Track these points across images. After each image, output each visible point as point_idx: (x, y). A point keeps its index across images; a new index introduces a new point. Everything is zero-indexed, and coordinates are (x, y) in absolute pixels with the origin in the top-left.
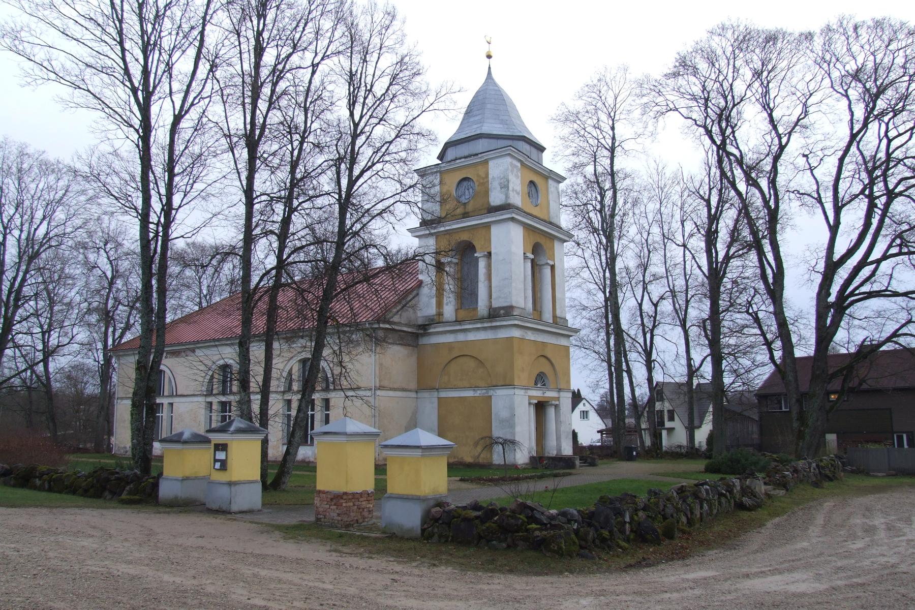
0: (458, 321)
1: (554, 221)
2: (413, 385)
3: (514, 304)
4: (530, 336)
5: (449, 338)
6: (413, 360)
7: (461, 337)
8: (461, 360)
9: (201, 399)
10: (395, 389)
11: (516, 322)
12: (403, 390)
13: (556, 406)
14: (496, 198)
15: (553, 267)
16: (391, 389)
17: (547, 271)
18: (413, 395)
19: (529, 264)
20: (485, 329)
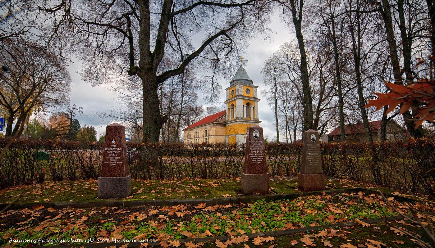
1: (255, 97)
5: (230, 124)
6: (225, 129)
12: (222, 135)
14: (237, 94)
15: (254, 108)
17: (252, 109)
19: (245, 108)
20: (235, 122)
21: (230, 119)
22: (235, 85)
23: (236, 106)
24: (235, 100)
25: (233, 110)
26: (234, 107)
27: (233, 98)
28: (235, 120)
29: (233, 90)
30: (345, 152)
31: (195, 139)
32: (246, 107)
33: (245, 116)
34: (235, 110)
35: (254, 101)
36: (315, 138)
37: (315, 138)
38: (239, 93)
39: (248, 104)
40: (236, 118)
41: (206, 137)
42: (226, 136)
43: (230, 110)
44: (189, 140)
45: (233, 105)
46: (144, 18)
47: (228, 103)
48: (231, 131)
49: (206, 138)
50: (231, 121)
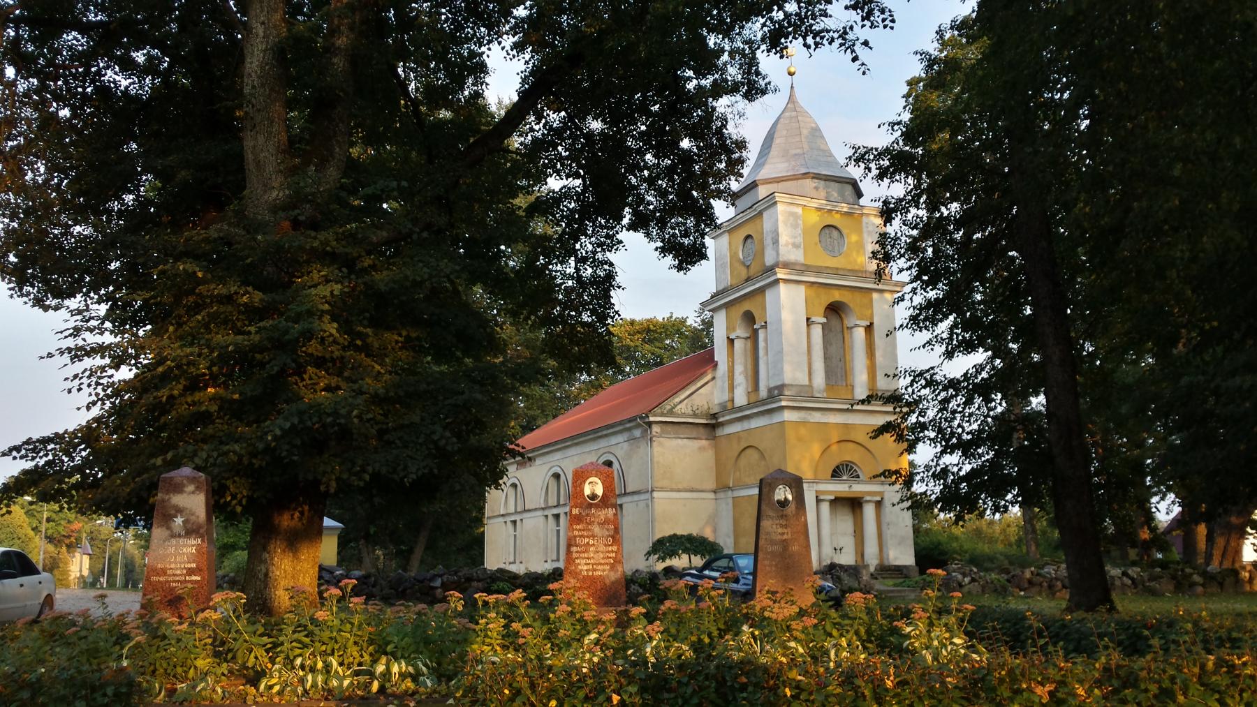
0: (750, 405)
2: (711, 484)
3: (786, 382)
4: (817, 417)
7: (746, 425)
8: (749, 451)
9: (539, 513)
10: (679, 491)
11: (784, 403)
13: (879, 504)
16: (672, 490)
17: (860, 333)
18: (712, 495)
19: (817, 331)
21: (741, 399)
22: (759, 207)
23: (765, 327)
24: (761, 290)
25: (749, 343)
26: (756, 332)
27: (748, 280)
28: (763, 402)
29: (748, 237)
30: (469, 580)
31: (550, 512)
32: (823, 325)
33: (819, 380)
34: (761, 344)
35: (761, 290)
36: (790, 497)
37: (790, 497)
38: (782, 250)
39: (835, 310)
40: (770, 390)
41: (555, 511)
42: (721, 495)
43: (737, 344)
44: (517, 518)
45: (749, 318)
46: (263, 23)
47: (727, 306)
48: (743, 461)
49: (557, 516)
50: (741, 409)
